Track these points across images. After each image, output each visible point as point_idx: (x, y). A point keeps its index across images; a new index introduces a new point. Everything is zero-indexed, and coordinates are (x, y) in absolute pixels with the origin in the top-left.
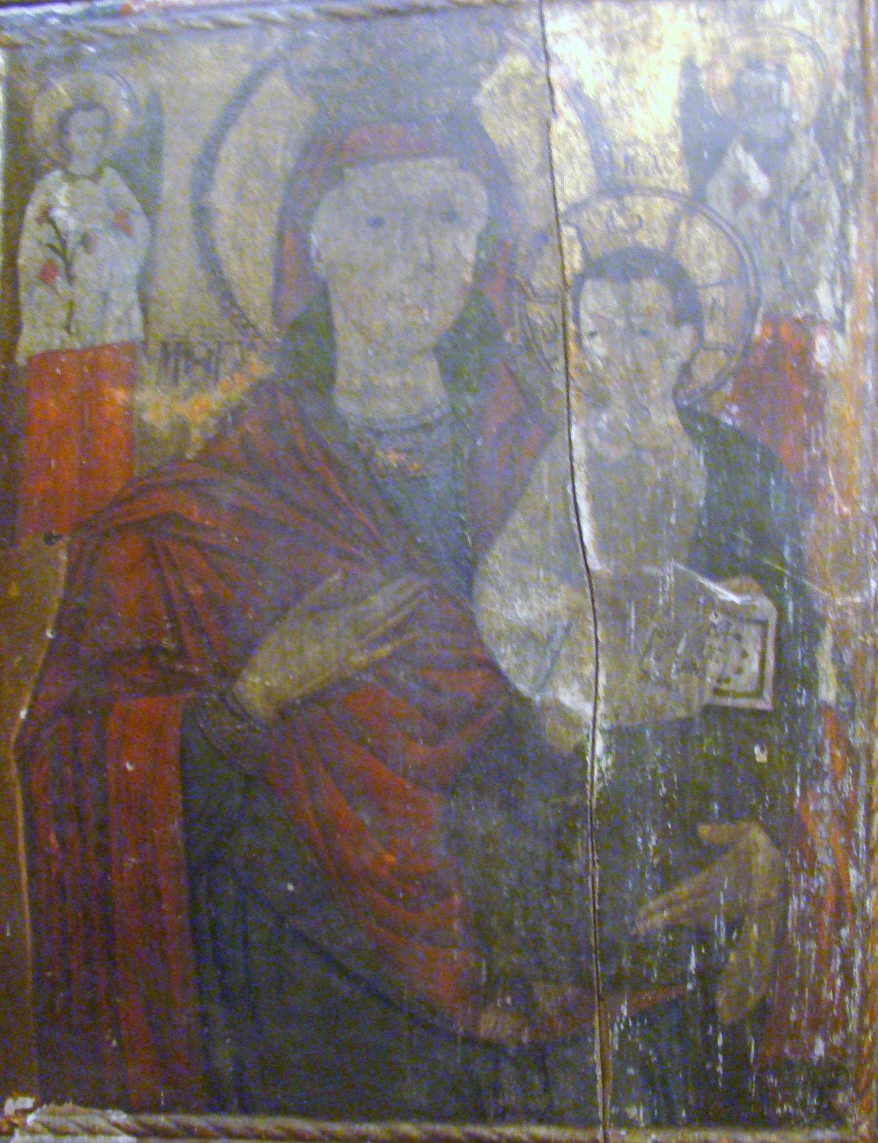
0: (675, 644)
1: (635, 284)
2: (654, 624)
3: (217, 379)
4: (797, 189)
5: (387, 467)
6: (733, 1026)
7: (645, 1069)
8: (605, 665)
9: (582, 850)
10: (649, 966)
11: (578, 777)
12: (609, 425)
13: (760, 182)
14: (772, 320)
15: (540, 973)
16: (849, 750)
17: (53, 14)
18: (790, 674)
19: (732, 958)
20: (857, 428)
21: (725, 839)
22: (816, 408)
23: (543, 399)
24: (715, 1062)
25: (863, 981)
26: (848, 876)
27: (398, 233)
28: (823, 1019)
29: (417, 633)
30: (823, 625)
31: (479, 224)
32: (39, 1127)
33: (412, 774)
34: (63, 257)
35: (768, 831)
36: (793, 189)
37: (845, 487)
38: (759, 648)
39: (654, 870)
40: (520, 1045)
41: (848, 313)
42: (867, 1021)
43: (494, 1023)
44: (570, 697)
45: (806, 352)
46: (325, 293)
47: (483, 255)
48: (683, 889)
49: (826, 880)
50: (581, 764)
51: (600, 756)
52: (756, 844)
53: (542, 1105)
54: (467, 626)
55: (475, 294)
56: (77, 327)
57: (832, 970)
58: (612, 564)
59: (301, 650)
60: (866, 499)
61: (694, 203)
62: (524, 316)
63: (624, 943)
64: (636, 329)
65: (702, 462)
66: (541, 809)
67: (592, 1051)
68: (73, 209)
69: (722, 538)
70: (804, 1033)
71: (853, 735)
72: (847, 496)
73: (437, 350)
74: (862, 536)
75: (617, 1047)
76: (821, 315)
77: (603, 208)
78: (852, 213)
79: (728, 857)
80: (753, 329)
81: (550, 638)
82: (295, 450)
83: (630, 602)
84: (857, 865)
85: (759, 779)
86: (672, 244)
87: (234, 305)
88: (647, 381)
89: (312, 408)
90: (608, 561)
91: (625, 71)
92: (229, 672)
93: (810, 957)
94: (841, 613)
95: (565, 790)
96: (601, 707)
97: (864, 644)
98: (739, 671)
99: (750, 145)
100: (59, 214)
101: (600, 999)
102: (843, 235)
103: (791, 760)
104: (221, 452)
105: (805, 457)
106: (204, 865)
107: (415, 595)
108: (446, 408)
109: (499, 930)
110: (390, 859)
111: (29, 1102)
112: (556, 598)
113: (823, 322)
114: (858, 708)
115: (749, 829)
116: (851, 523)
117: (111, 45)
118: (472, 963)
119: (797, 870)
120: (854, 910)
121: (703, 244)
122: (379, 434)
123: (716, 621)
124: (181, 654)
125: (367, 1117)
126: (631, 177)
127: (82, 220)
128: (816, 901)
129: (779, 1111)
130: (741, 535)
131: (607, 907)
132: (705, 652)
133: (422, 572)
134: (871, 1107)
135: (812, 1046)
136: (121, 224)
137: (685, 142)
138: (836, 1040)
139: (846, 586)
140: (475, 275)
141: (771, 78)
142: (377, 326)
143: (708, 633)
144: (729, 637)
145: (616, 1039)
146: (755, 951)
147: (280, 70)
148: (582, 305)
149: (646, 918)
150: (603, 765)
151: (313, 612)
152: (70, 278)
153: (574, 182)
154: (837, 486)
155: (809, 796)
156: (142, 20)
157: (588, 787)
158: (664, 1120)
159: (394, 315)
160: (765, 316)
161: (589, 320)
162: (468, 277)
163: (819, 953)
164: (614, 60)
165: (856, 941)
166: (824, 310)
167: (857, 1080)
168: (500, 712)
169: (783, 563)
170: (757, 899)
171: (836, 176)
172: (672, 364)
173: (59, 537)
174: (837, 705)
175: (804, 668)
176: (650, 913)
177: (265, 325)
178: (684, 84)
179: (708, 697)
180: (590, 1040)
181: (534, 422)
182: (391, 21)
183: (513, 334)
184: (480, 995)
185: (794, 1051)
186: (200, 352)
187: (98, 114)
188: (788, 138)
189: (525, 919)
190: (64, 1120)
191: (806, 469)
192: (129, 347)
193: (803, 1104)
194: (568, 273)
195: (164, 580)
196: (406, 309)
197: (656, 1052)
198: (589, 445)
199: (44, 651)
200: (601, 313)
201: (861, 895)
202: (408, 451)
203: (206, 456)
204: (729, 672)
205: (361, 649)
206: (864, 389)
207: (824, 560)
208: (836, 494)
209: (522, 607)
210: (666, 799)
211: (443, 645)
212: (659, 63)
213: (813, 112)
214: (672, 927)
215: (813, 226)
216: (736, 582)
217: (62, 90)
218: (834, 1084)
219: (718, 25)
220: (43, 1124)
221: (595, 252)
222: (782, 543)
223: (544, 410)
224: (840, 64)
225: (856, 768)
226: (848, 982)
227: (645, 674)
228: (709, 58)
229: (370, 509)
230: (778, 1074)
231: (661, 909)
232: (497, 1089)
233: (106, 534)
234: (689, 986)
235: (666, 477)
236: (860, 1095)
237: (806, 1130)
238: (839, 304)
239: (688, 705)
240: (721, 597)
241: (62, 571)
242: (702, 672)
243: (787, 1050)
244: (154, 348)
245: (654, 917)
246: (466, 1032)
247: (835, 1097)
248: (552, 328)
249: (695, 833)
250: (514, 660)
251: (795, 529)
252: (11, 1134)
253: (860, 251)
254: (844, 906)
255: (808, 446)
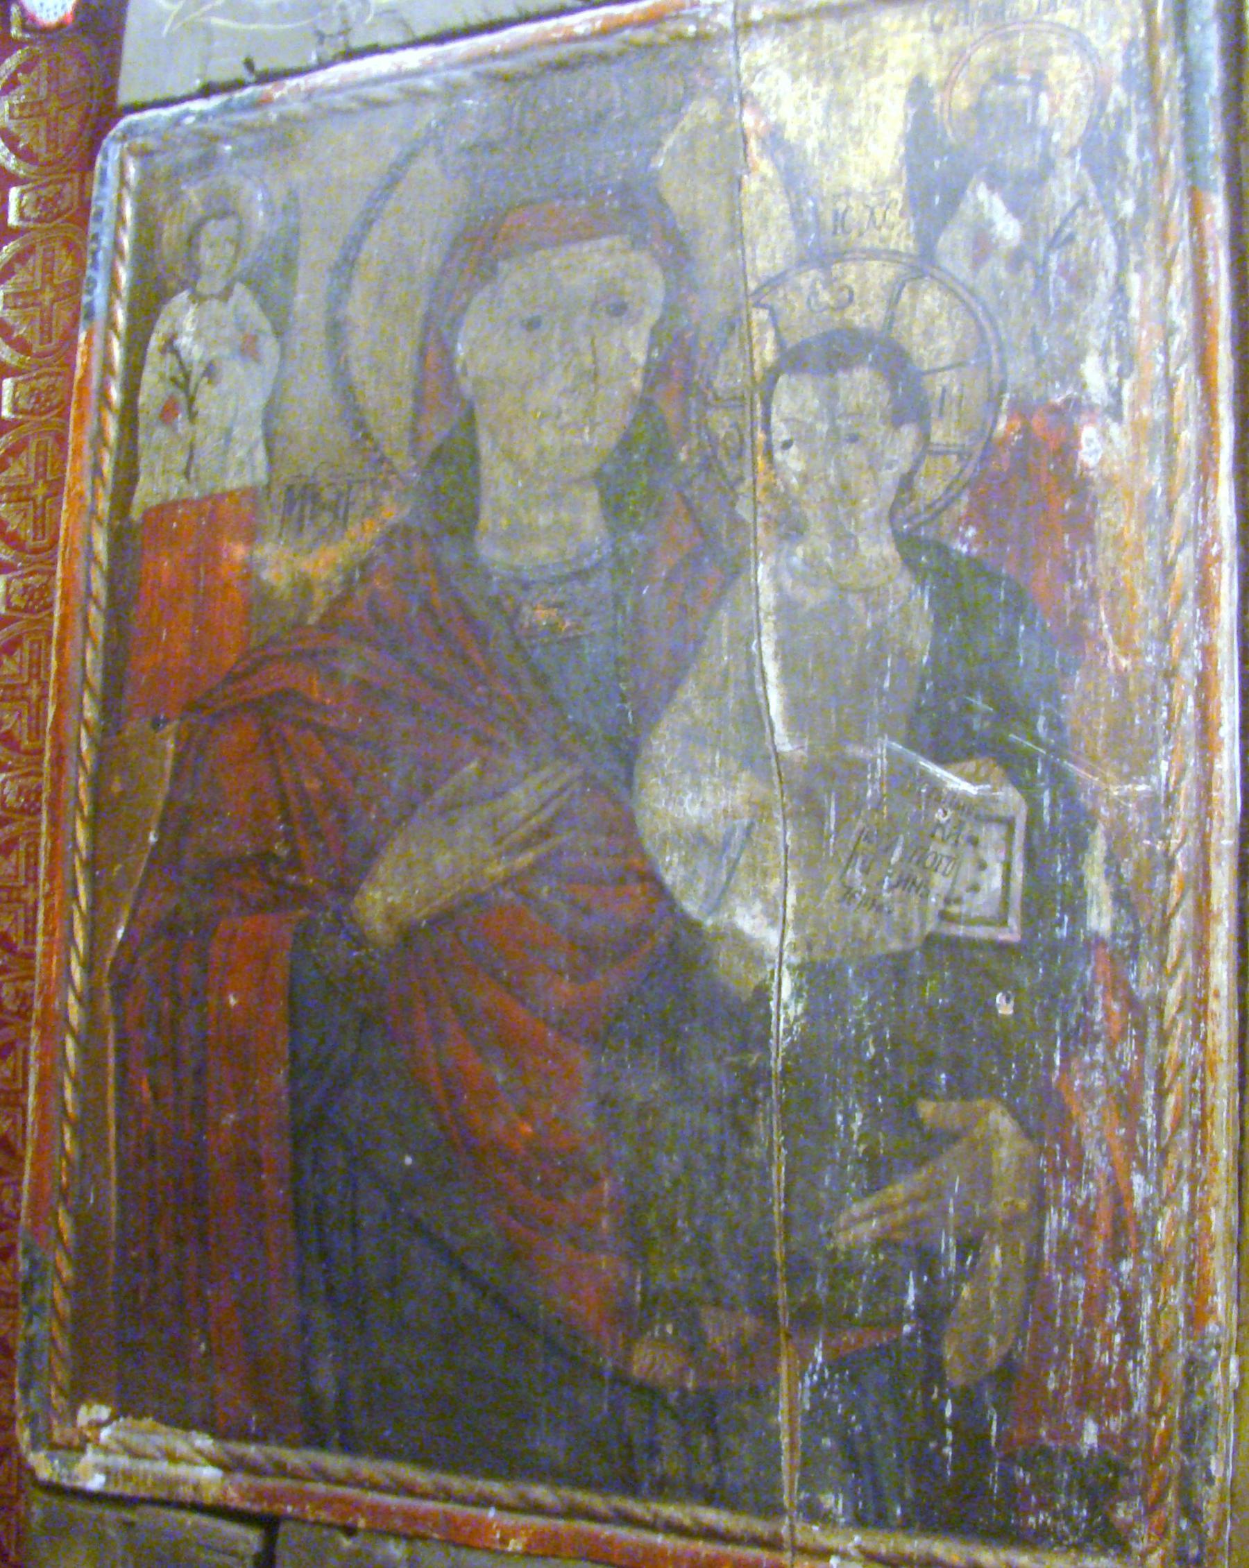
0: (889, 849)
1: (841, 375)
2: (860, 824)
3: (345, 528)
4: (1058, 232)
5: (534, 627)
6: (966, 1390)
7: (846, 1442)
8: (794, 878)
9: (768, 1130)
10: (852, 1296)
11: (758, 1029)
12: (805, 561)
13: (1008, 229)
14: (1021, 410)
15: (709, 1295)
16: (1131, 1003)
17: (187, 113)
18: (1048, 895)
19: (966, 1292)
20: (1139, 548)
21: (957, 1124)
22: (1082, 526)
23: (723, 529)
24: (942, 1443)
25: (1153, 1340)
26: (1130, 1184)
27: (557, 335)
28: (1096, 1393)
29: (563, 837)
30: (1094, 826)
31: (651, 316)
32: (114, 1446)
33: (554, 1018)
34: (187, 392)
35: (1017, 1114)
36: (1052, 233)
37: (1123, 632)
38: (1002, 856)
39: (859, 1161)
40: (683, 1391)
41: (1126, 393)
42: (1158, 1399)
43: (646, 1360)
44: (749, 920)
45: (1067, 450)
46: (470, 417)
47: (655, 355)
48: (898, 1190)
49: (1099, 1189)
50: (762, 1011)
51: (788, 1004)
52: (997, 1131)
53: (710, 1479)
54: (623, 828)
55: (645, 404)
56: (197, 472)
57: (1108, 1320)
58: (806, 743)
59: (429, 859)
60: (1153, 646)
61: (922, 265)
62: (702, 425)
63: (819, 1259)
64: (843, 433)
65: (926, 606)
66: (713, 1072)
67: (775, 1410)
68: (198, 335)
69: (953, 708)
70: (1069, 1409)
71: (1137, 980)
72: (1126, 644)
73: (598, 476)
74: (1149, 698)
75: (808, 1407)
76: (1088, 398)
77: (804, 281)
78: (1134, 258)
79: (958, 1148)
80: (995, 422)
81: (726, 844)
82: (427, 607)
83: (830, 792)
84: (1144, 1170)
85: (1000, 1041)
86: (891, 319)
87: (367, 436)
88: (855, 502)
89: (451, 556)
90: (801, 738)
91: (839, 103)
92: (347, 887)
93: (1076, 1298)
94: (1118, 804)
95: (744, 1048)
96: (790, 936)
97: (1151, 851)
98: (975, 888)
99: (994, 182)
100: (184, 342)
101: (788, 1336)
102: (1120, 288)
103: (1047, 1012)
104: (350, 614)
105: (1067, 589)
106: (308, 1130)
107: (563, 789)
108: (607, 549)
109: (657, 1233)
110: (527, 1129)
111: (104, 1412)
112: (734, 788)
113: (1092, 408)
114: (1143, 942)
115: (987, 1112)
116: (1131, 682)
117: (248, 141)
118: (624, 1274)
119: (1057, 1172)
120: (1140, 1235)
121: (931, 318)
122: (526, 586)
123: (943, 820)
124: (294, 863)
125: (491, 1474)
126: (840, 238)
127: (207, 346)
128: (1083, 1217)
129: (1032, 1520)
130: (979, 703)
131: (796, 1209)
132: (928, 863)
133: (573, 759)
134: (1166, 1528)
135: (1079, 1434)
136: (248, 349)
137: (910, 185)
138: (1115, 1424)
139: (1126, 768)
140: (645, 380)
141: (1025, 91)
142: (529, 454)
143: (933, 835)
144: (961, 841)
145: (807, 1394)
146: (996, 1284)
147: (431, 150)
148: (774, 410)
149: (846, 1229)
150: (791, 1012)
151: (444, 810)
152: (192, 416)
153: (769, 251)
154: (1111, 630)
155: (1074, 1065)
156: (283, 108)
157: (772, 1042)
158: (871, 1517)
159: (549, 437)
160: (1013, 404)
161: (782, 426)
162: (637, 383)
163: (1089, 1296)
164: (824, 91)
165: (1143, 1279)
166: (1091, 390)
167: (1146, 1488)
168: (663, 940)
169: (1036, 740)
170: (1000, 1208)
171: (1111, 211)
172: (889, 477)
173: (167, 721)
174: (1114, 936)
175: (1064, 885)
176: (854, 1221)
177: (403, 461)
178: (911, 112)
179: (930, 927)
180: (773, 1393)
181: (714, 561)
182: (558, 78)
183: (689, 452)
184: (631, 1320)
185: (1052, 1436)
186: (328, 495)
187: (231, 222)
188: (1048, 165)
189: (690, 1217)
190: (142, 1439)
191: (1069, 609)
192: (251, 493)
193: (1067, 1513)
194: (757, 368)
195: (277, 772)
196: (562, 428)
197: (861, 1420)
198: (779, 588)
199: (146, 857)
200: (799, 416)
201: (1150, 1213)
202: (559, 605)
203: (329, 623)
204: (960, 890)
205: (499, 856)
206: (1152, 492)
207: (1093, 733)
208: (1110, 641)
209: (692, 801)
210: (874, 1063)
211: (596, 853)
212: (881, 89)
213: (1080, 129)
214: (882, 1243)
215: (1079, 282)
216: (971, 766)
217: (195, 200)
218: (1111, 1488)
219: (958, 31)
220: (118, 1441)
221: (792, 340)
222: (1035, 711)
223: (725, 545)
224: (1118, 63)
225: (1141, 1026)
226: (1132, 1341)
227: (848, 893)
228: (944, 74)
229: (514, 681)
230: (1029, 1465)
231: (868, 1217)
232: (653, 1450)
233: (220, 716)
234: (907, 1329)
235: (879, 626)
236: (1151, 1509)
237: (1073, 1553)
238: (1115, 381)
239: (906, 937)
240: (950, 786)
241: (169, 764)
242: (924, 890)
243: (1043, 1432)
244: (278, 493)
245: (858, 1226)
246: (616, 1368)
247: (1114, 1509)
248: (737, 439)
249: (913, 1112)
250: (682, 871)
251: (1052, 693)
252: (82, 1450)
253: (1143, 305)
254: (1124, 1230)
255: (1072, 579)
